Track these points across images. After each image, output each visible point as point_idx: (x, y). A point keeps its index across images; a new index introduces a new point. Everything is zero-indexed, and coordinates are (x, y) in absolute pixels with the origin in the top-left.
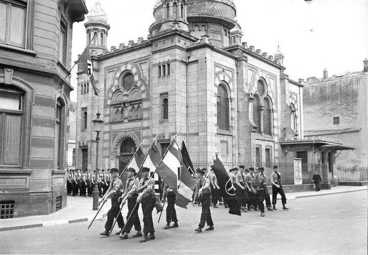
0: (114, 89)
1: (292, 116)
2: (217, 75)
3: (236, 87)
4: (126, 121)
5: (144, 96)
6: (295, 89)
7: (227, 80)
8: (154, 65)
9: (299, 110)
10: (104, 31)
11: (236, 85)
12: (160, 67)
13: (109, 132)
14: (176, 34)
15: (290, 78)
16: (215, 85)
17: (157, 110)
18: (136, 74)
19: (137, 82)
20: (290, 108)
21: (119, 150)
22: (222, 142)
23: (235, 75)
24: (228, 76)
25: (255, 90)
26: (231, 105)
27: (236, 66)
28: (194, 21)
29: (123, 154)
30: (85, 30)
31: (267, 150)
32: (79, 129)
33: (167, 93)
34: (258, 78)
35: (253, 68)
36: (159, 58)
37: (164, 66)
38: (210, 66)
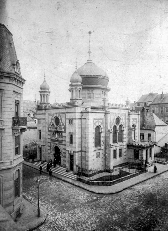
0: (51, 124)
5: (63, 130)
9: (138, 129)
12: (69, 120)
19: (61, 123)
26: (102, 135)
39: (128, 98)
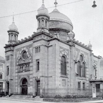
0: (19, 58)
1: (94, 70)
2: (61, 52)
3: (70, 57)
4: (24, 71)
5: (30, 61)
6: (96, 59)
7: (66, 54)
8: (34, 48)
10: (16, 34)
11: (70, 56)
13: (18, 76)
14: (43, 34)
15: (94, 55)
16: (60, 56)
17: (35, 67)
18: (27, 52)
19: (28, 55)
20: (94, 67)
21: (21, 83)
22: (63, 80)
23: (70, 52)
24: (66, 52)
25: (78, 59)
27: (70, 48)
28: (51, 30)
29: (23, 85)
30: (8, 33)
31: (84, 83)
32: (6, 75)
33: (39, 59)
34: (80, 54)
35: (77, 50)
36: (36, 44)
37: (38, 48)
38: (57, 48)
39: (90, 42)
